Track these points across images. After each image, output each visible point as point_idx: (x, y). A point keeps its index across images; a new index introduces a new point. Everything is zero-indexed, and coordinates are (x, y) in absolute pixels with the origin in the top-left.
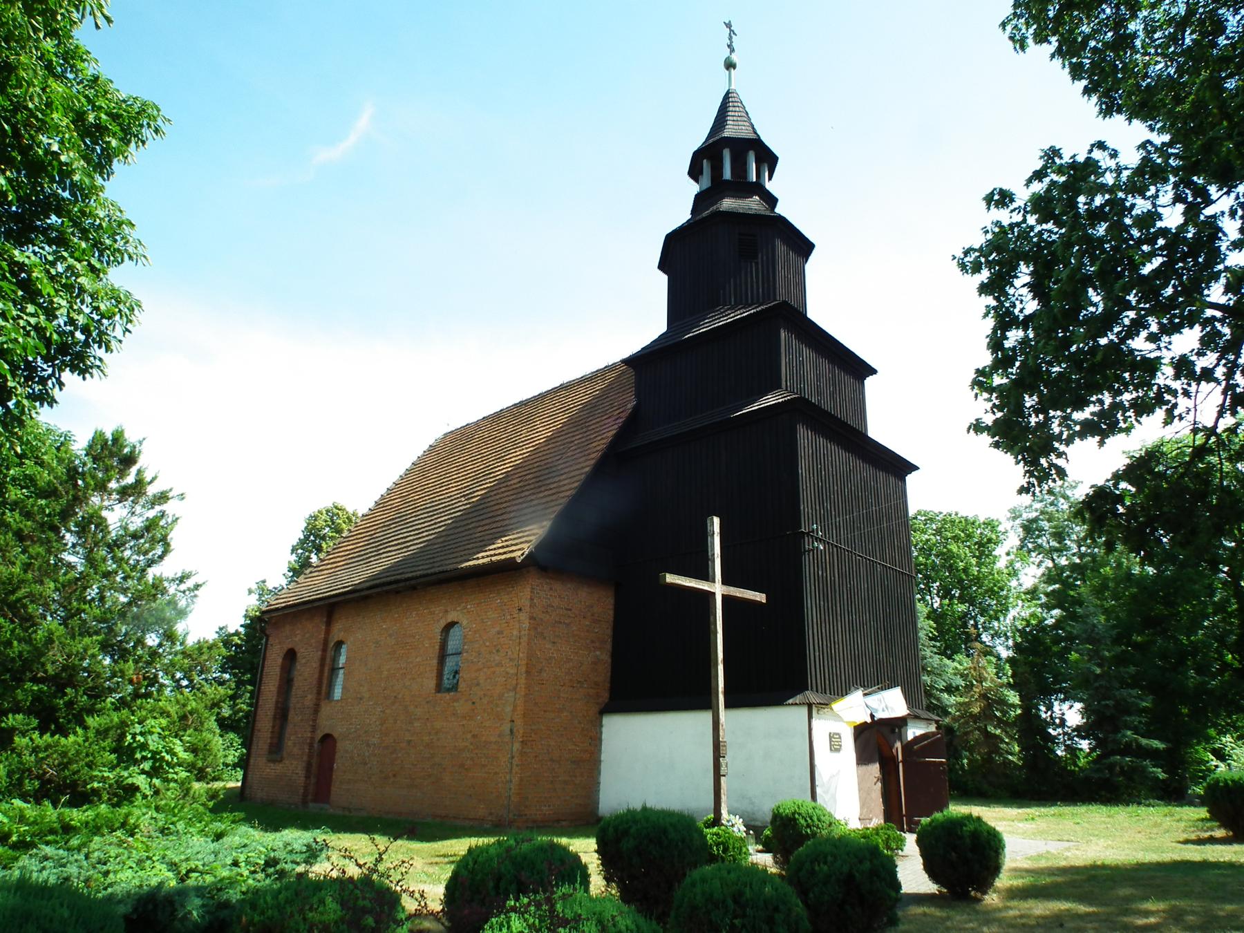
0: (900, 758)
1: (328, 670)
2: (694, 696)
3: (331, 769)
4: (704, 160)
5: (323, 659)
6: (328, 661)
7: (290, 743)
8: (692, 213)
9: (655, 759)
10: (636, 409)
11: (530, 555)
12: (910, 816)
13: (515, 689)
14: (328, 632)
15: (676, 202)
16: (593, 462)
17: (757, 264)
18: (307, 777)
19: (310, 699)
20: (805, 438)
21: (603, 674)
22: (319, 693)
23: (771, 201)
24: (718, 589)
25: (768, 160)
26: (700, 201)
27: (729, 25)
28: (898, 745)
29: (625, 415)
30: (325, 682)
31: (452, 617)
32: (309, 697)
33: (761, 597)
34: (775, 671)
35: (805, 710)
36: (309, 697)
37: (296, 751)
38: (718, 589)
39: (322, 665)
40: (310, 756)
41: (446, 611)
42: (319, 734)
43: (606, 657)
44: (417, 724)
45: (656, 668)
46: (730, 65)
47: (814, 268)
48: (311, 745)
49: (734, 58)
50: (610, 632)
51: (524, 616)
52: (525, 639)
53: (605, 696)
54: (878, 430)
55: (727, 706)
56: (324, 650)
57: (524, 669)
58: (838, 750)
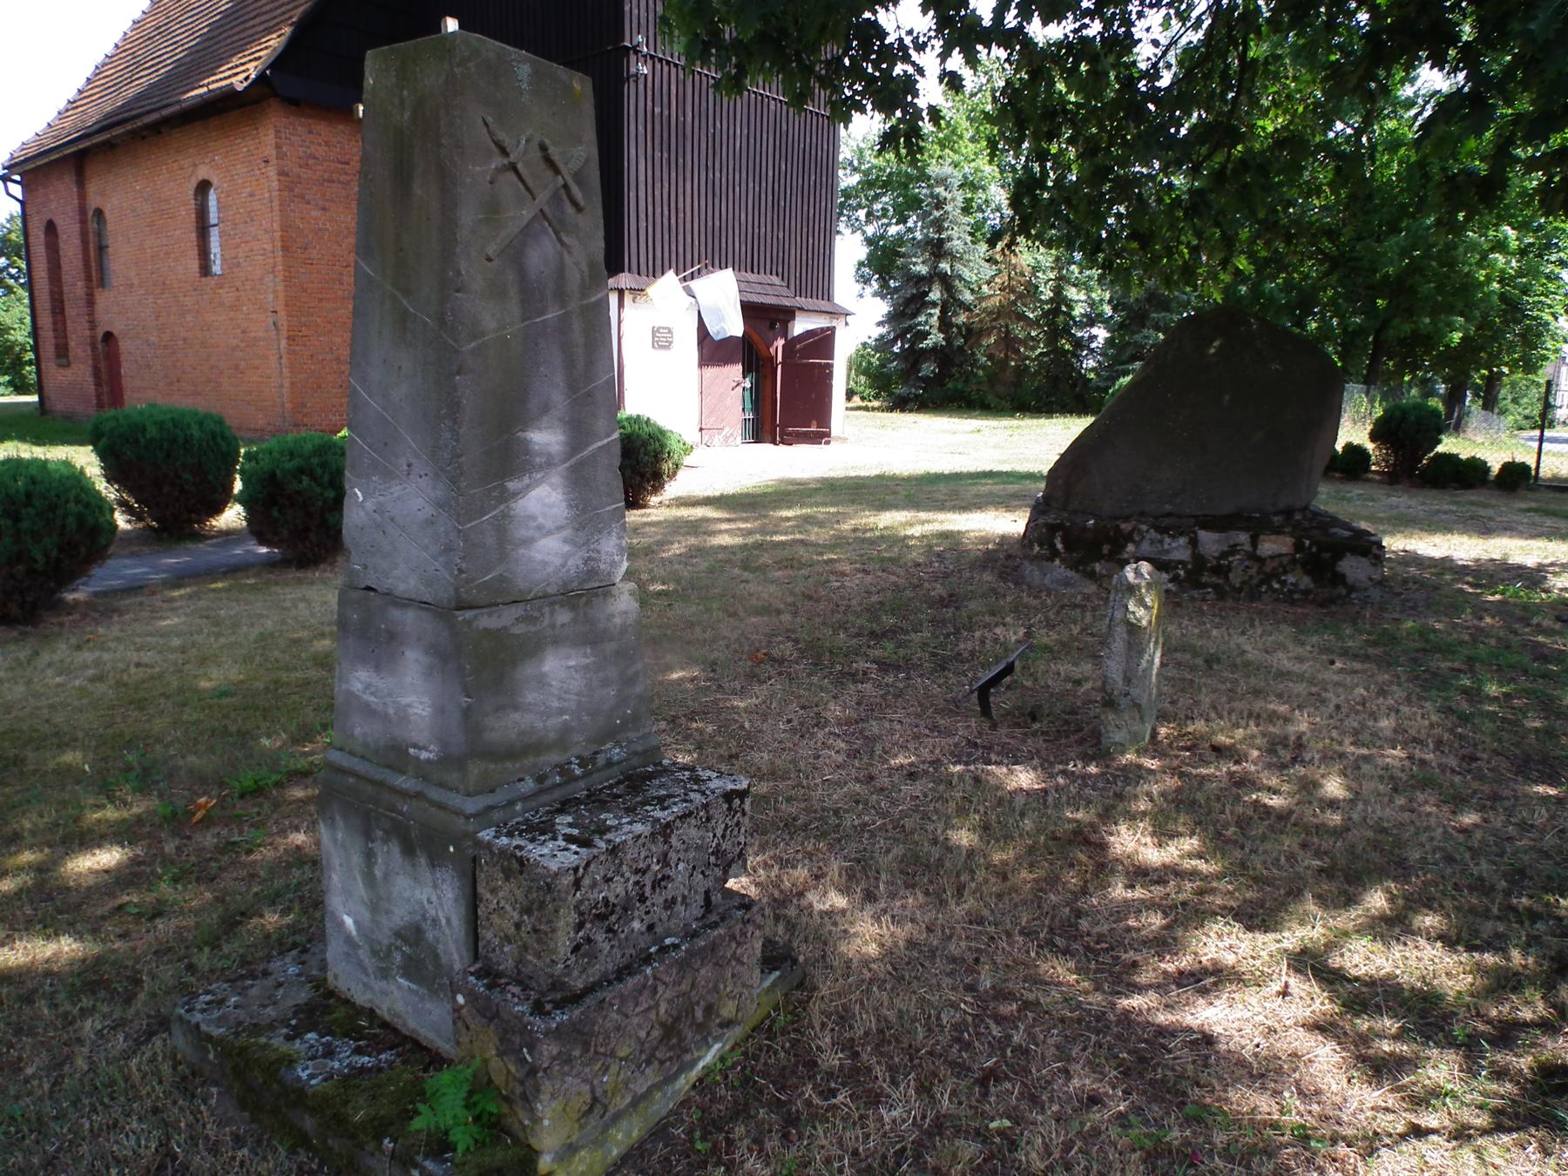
0: (780, 359)
3: (119, 373)
11: (261, 77)
12: (784, 426)
14: (82, 196)
18: (98, 384)
22: (88, 278)
28: (780, 343)
31: (203, 173)
40: (95, 359)
41: (195, 165)
42: (100, 333)
44: (189, 318)
48: (93, 346)
51: (272, 172)
52: (276, 203)
56: (83, 222)
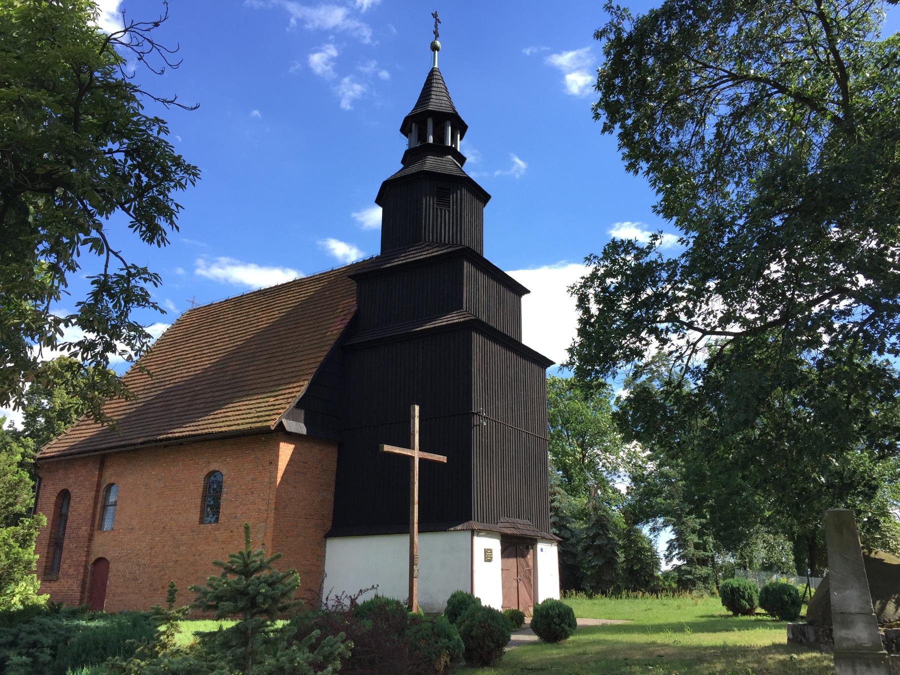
1: (100, 506)
2: (400, 526)
3: (104, 585)
4: (413, 124)
5: (96, 498)
6: (101, 499)
7: (65, 566)
8: (403, 162)
9: (362, 569)
10: (357, 312)
13: (266, 521)
14: (100, 476)
15: (389, 156)
16: (326, 353)
17: (449, 211)
18: (82, 592)
19: (84, 530)
20: (477, 339)
21: (329, 509)
22: (93, 525)
23: (462, 159)
24: (416, 454)
25: (461, 127)
26: (409, 157)
27: (435, 15)
29: (349, 317)
30: (98, 516)
32: (84, 528)
33: (443, 459)
34: (450, 508)
35: (470, 534)
36: (84, 528)
37: (71, 571)
38: (416, 454)
39: (96, 503)
40: (85, 576)
41: (209, 462)
42: (93, 558)
43: (331, 497)
45: (366, 504)
46: (434, 48)
47: (488, 211)
49: (438, 43)
50: (334, 478)
53: (329, 524)
54: (529, 339)
55: (420, 531)
56: (98, 491)
57: (273, 507)
58: (490, 561)
